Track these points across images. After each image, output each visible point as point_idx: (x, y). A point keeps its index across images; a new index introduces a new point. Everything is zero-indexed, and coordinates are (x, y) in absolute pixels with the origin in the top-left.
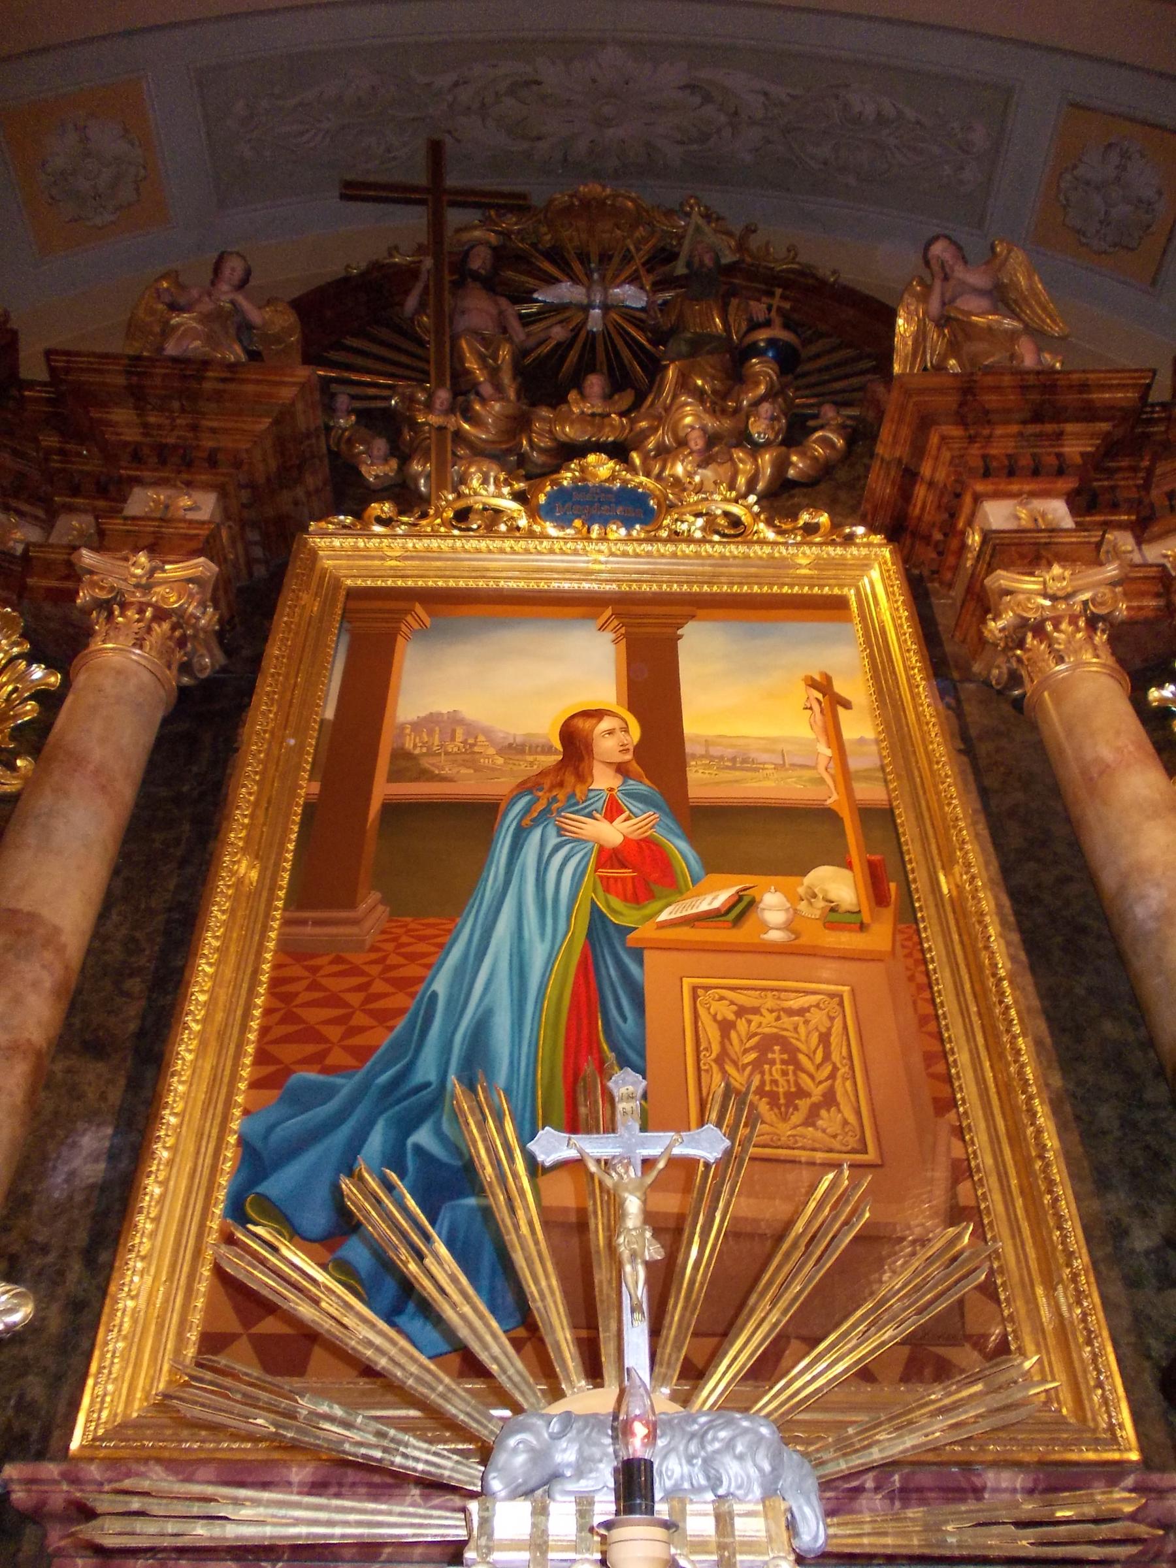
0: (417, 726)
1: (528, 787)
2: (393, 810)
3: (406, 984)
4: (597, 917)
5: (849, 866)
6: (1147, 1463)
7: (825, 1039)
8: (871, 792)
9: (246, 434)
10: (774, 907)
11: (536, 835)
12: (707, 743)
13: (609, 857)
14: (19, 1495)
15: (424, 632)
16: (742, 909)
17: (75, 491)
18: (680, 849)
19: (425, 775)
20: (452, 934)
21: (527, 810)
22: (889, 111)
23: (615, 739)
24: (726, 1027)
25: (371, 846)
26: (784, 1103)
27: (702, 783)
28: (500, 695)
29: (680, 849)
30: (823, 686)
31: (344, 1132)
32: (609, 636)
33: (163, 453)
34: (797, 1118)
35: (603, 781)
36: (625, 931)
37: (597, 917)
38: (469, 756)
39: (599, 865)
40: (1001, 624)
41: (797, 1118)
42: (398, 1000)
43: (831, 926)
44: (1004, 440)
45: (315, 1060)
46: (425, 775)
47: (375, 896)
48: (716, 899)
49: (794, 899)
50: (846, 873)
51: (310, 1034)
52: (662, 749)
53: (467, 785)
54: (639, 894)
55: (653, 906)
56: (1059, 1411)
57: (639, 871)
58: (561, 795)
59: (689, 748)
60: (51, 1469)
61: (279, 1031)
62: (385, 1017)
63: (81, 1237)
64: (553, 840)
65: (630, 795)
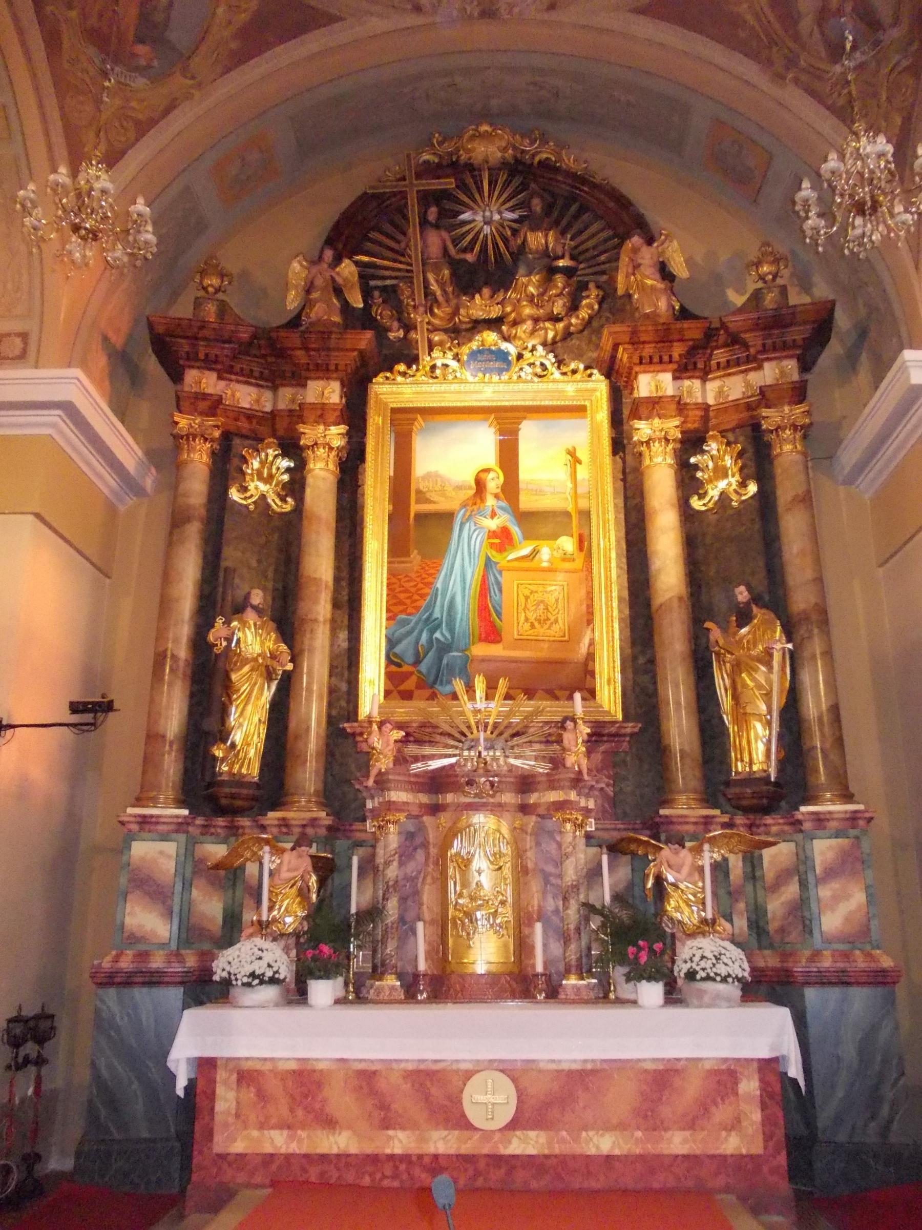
1: (464, 505)
2: (420, 517)
3: (429, 585)
4: (488, 560)
5: (572, 536)
6: (623, 721)
7: (557, 600)
8: (583, 504)
9: (347, 360)
10: (545, 554)
11: (467, 525)
12: (527, 483)
13: (492, 534)
14: (349, 730)
15: (422, 429)
16: (535, 552)
17: (284, 378)
18: (515, 531)
21: (464, 515)
23: (494, 482)
24: (527, 598)
25: (412, 533)
27: (526, 502)
28: (452, 459)
29: (515, 531)
30: (572, 453)
31: (415, 633)
32: (492, 430)
33: (318, 367)
34: (546, 627)
35: (490, 502)
36: (497, 563)
37: (488, 560)
38: (442, 492)
39: (489, 538)
41: (546, 627)
42: (426, 591)
43: (564, 560)
44: (648, 350)
45: (404, 611)
47: (416, 552)
48: (526, 551)
49: (552, 550)
50: (570, 539)
51: (400, 603)
52: (511, 488)
53: (442, 505)
54: (501, 549)
55: (505, 554)
58: (475, 508)
59: (521, 485)
60: (355, 724)
61: (392, 602)
62: (423, 596)
63: (346, 663)
64: (473, 528)
65: (501, 508)
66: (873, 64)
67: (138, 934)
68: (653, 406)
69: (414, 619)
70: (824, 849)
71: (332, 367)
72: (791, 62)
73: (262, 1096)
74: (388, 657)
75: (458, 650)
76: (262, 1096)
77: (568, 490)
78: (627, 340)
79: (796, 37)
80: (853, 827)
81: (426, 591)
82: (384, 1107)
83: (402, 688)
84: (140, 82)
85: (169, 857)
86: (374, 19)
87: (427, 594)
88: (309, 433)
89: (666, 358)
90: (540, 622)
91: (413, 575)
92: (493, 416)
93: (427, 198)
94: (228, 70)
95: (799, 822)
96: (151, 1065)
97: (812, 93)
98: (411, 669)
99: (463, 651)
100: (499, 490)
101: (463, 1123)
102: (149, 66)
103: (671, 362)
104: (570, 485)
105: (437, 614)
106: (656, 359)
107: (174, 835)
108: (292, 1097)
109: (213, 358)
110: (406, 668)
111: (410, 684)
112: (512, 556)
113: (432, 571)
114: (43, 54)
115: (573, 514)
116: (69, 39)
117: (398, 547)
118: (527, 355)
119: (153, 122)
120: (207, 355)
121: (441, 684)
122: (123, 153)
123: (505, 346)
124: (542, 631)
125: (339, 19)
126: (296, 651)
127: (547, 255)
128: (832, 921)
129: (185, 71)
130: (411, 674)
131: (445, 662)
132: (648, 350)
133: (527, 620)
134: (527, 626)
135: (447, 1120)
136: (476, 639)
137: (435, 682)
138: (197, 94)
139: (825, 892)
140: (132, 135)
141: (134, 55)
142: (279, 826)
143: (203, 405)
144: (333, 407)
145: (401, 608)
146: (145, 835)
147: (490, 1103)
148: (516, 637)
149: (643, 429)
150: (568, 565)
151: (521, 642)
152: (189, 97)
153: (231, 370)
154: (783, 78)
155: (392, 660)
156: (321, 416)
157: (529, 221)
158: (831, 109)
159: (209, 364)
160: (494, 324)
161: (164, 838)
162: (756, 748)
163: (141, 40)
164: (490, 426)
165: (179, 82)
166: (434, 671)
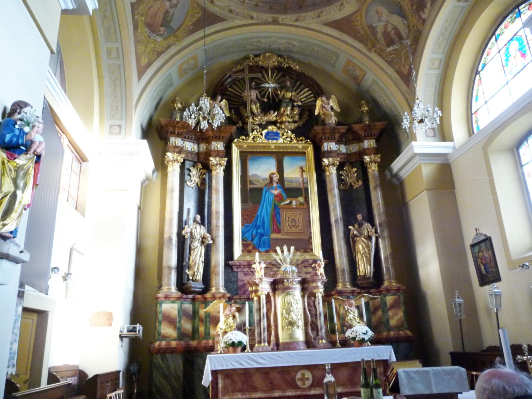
0: (252, 176)
1: (266, 185)
2: (251, 189)
3: (255, 213)
4: (275, 204)
9: (228, 135)
13: (276, 196)
16: (291, 203)
19: (253, 184)
20: (259, 207)
22: (320, 50)
23: (276, 178)
24: (289, 218)
26: (294, 226)
27: (287, 185)
29: (284, 194)
32: (274, 160)
35: (275, 185)
38: (258, 181)
40: (384, 16)
42: (254, 215)
45: (247, 222)
46: (253, 184)
48: (288, 202)
49: (296, 201)
52: (282, 180)
53: (259, 186)
56: (354, 226)
57: (279, 198)
59: (285, 179)
62: (254, 217)
65: (279, 187)
66: (400, 50)
67: (166, 335)
68: (329, 154)
69: (251, 225)
70: (389, 299)
71: (221, 137)
72: (374, 46)
73: (233, 382)
74: (242, 238)
76: (233, 382)
79: (376, 39)
80: (398, 292)
82: (271, 382)
83: (247, 249)
84: (160, 39)
85: (175, 309)
86: (238, 20)
88: (213, 160)
89: (333, 138)
93: (252, 79)
94: (188, 35)
95: (381, 291)
96: (173, 380)
97: (379, 55)
101: (297, 387)
102: (164, 34)
103: (335, 139)
104: (301, 179)
105: (258, 223)
106: (330, 138)
107: (177, 301)
108: (243, 382)
109: (180, 133)
110: (249, 242)
111: (250, 248)
112: (282, 204)
114: (132, 31)
116: (141, 25)
117: (244, 201)
118: (285, 134)
119: (162, 52)
120: (178, 133)
122: (153, 62)
123: (279, 131)
125: (227, 20)
126: (214, 236)
127: (292, 101)
128: (393, 322)
129: (175, 36)
131: (262, 240)
132: (328, 135)
133: (289, 225)
134: (289, 228)
135: (291, 385)
138: (177, 43)
139: (390, 313)
140: (156, 56)
141: (159, 31)
142: (212, 297)
143: (177, 150)
144: (222, 151)
146: (166, 301)
147: (273, 146)
149: (326, 161)
150: (302, 207)
151: (287, 233)
152: (175, 44)
153: (185, 137)
154: (371, 50)
155: (244, 239)
156: (218, 154)
157: (283, 87)
158: (386, 61)
159: (179, 135)
160: (274, 123)
161: (173, 302)
162: (365, 268)
163: (162, 26)
165: (172, 39)
166: (258, 244)
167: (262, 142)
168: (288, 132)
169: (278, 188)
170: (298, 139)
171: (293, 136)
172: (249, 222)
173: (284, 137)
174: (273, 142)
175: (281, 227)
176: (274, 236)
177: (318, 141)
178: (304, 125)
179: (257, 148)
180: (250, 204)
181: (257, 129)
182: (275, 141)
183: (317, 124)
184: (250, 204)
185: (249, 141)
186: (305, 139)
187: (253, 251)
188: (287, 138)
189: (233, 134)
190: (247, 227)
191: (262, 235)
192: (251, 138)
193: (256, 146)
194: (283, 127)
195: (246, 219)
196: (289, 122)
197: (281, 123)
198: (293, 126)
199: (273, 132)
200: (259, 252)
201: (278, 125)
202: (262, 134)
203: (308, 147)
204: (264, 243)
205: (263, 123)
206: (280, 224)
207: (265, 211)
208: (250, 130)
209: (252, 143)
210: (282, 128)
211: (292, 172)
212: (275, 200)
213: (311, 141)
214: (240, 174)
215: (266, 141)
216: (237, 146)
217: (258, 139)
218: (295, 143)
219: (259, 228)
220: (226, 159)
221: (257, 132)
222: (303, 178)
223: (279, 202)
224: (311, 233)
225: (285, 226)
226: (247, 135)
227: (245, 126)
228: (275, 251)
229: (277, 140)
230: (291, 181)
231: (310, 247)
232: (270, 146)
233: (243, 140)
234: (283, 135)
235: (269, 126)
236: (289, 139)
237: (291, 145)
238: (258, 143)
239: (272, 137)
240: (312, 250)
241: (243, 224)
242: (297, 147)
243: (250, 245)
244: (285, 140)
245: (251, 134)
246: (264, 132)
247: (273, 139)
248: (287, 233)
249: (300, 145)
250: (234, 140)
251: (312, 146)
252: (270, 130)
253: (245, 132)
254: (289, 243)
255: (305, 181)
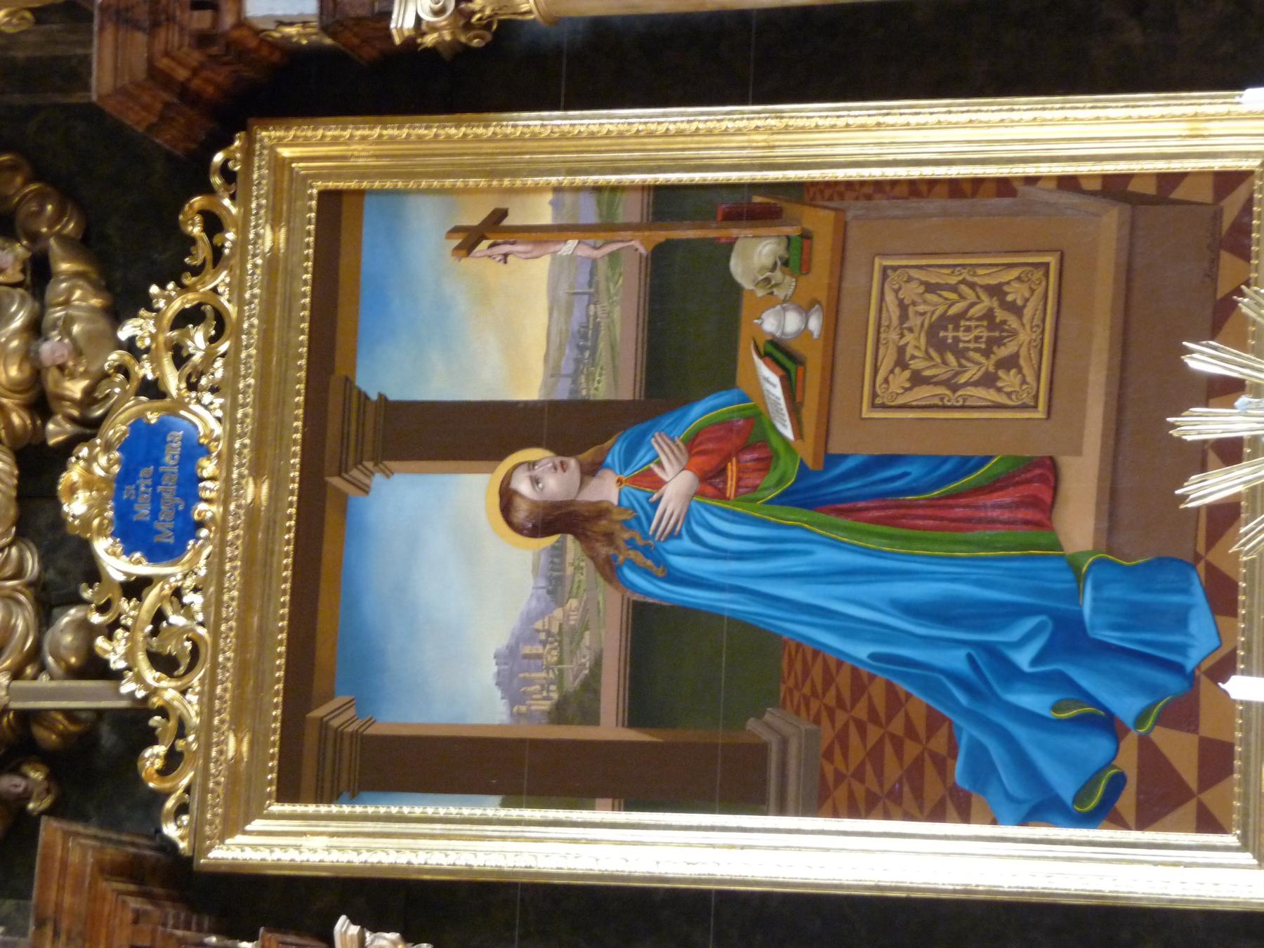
0: (514, 696)
1: (609, 570)
3: (860, 682)
5: (730, 245)
7: (930, 288)
10: (781, 322)
13: (710, 481)
16: (781, 354)
19: (591, 685)
21: (646, 572)
23: (544, 477)
24: (918, 379)
26: (997, 333)
27: (614, 381)
29: (700, 413)
34: (1013, 322)
35: (606, 489)
36: (803, 470)
38: (566, 639)
39: (721, 495)
41: (1013, 322)
42: (877, 693)
45: (942, 766)
46: (591, 685)
48: (771, 382)
49: (770, 301)
52: (569, 426)
53: (608, 640)
57: (730, 455)
59: (562, 393)
62: (895, 700)
64: (686, 543)
65: (627, 462)
69: (968, 733)
75: (1077, 594)
77: (585, 251)
78: (141, 37)
81: (877, 693)
83: (1191, 777)
87: (890, 687)
90: (999, 342)
91: (827, 733)
92: (335, 481)
98: (1130, 746)
99: (1079, 578)
100: (572, 463)
104: (569, 247)
105: (956, 660)
110: (1128, 761)
111: (1180, 750)
113: (817, 673)
115: (661, 236)
117: (738, 784)
118: (146, 370)
121: (1182, 649)
123: (117, 429)
124: (1024, 336)
130: (1146, 744)
133: (988, 381)
134: (1009, 380)
136: (1041, 537)
137: (1177, 669)
145: (930, 771)
147: (254, 492)
148: (1040, 414)
151: (1058, 394)
164: (365, 490)
167: (212, 584)
168: (131, 346)
169: (641, 460)
170: (202, 252)
171: (170, 300)
172: (939, 744)
173: (173, 381)
174: (210, 489)
175: (1002, 451)
176: (1078, 525)
177: (222, 76)
178: (67, 193)
179: (264, 634)
180: (772, 727)
181: (88, 631)
182: (208, 467)
183: (77, 74)
184: (772, 727)
185: (191, 707)
186: (208, 190)
187: (1208, 728)
188: (180, 359)
189: (111, 853)
190: (982, 767)
191: (1069, 637)
192: (169, 691)
193: (241, 647)
194: (76, 388)
195: (915, 775)
196: (36, 329)
197: (41, 403)
198: (75, 297)
199: (126, 477)
200: (1225, 667)
201: (56, 431)
202: (135, 588)
203: (281, 166)
204: (1136, 617)
205: (32, 565)
206: (967, 465)
207: (845, 597)
208: (89, 697)
209: (211, 681)
210: (90, 399)
211: (500, 326)
212: (747, 491)
213: (225, 143)
214: (491, 808)
215: (200, 554)
216: (232, 826)
217: (177, 620)
218: (237, 287)
219: (995, 654)
220: (345, 929)
221: (109, 631)
222: (559, 231)
223: (766, 463)
224: (1068, 183)
225: (992, 414)
226: (136, 724)
227: (47, 737)
228: (1225, 516)
229: (194, 450)
230: (583, 342)
231: (1205, 194)
232: (252, 511)
233: (173, 760)
234: (152, 389)
235: (59, 521)
236: (197, 340)
237: (252, 322)
238: (213, 625)
239: (168, 489)
240: (1228, 181)
241: (956, 805)
242: (272, 262)
243: (1150, 754)
244: (201, 382)
245: (127, 687)
246: (117, 564)
247: (190, 484)
248: (1058, 394)
249: (256, 245)
250: (169, 846)
251: (267, 135)
252: (97, 506)
253: (108, 738)
254: (1149, 388)
255: (589, 213)
